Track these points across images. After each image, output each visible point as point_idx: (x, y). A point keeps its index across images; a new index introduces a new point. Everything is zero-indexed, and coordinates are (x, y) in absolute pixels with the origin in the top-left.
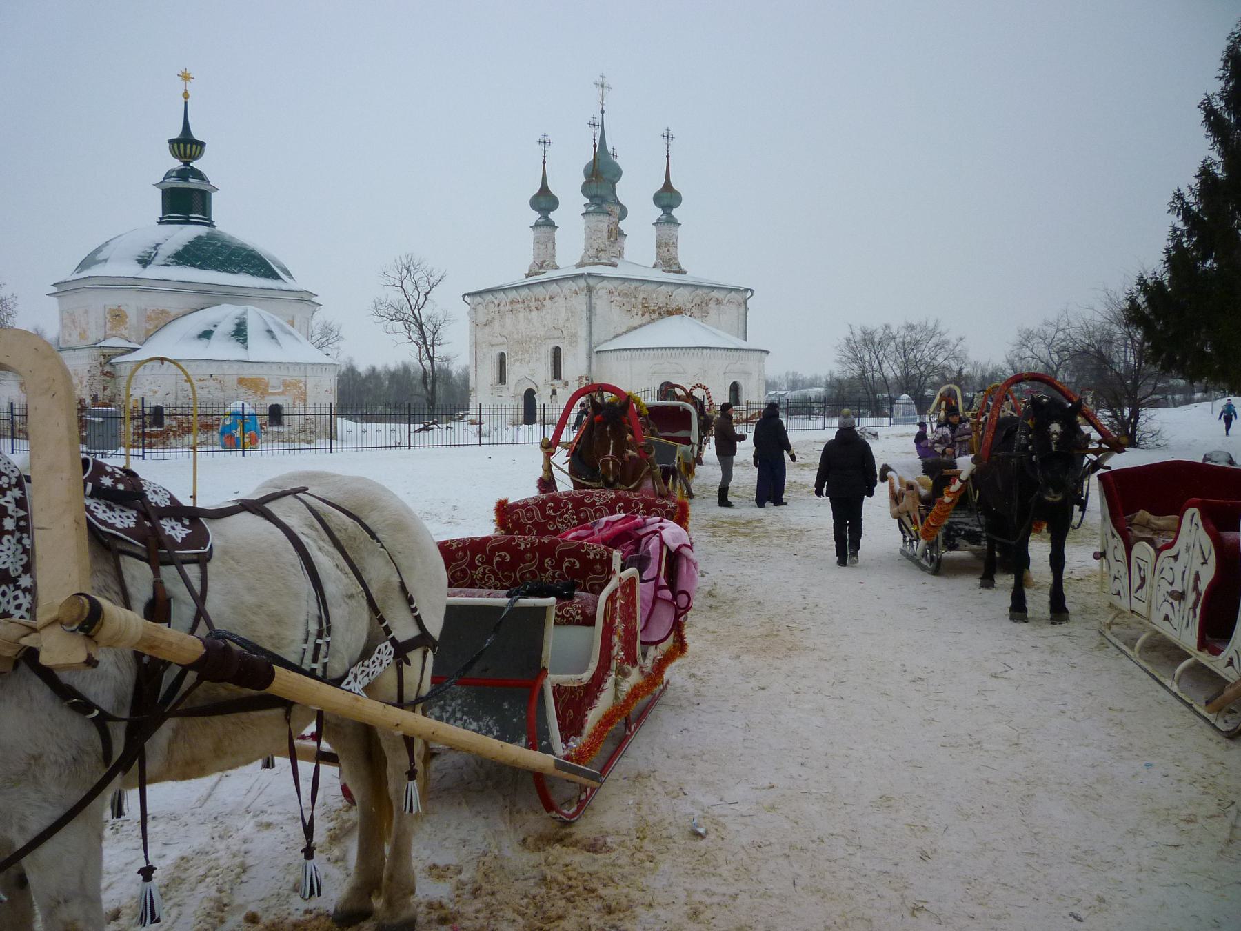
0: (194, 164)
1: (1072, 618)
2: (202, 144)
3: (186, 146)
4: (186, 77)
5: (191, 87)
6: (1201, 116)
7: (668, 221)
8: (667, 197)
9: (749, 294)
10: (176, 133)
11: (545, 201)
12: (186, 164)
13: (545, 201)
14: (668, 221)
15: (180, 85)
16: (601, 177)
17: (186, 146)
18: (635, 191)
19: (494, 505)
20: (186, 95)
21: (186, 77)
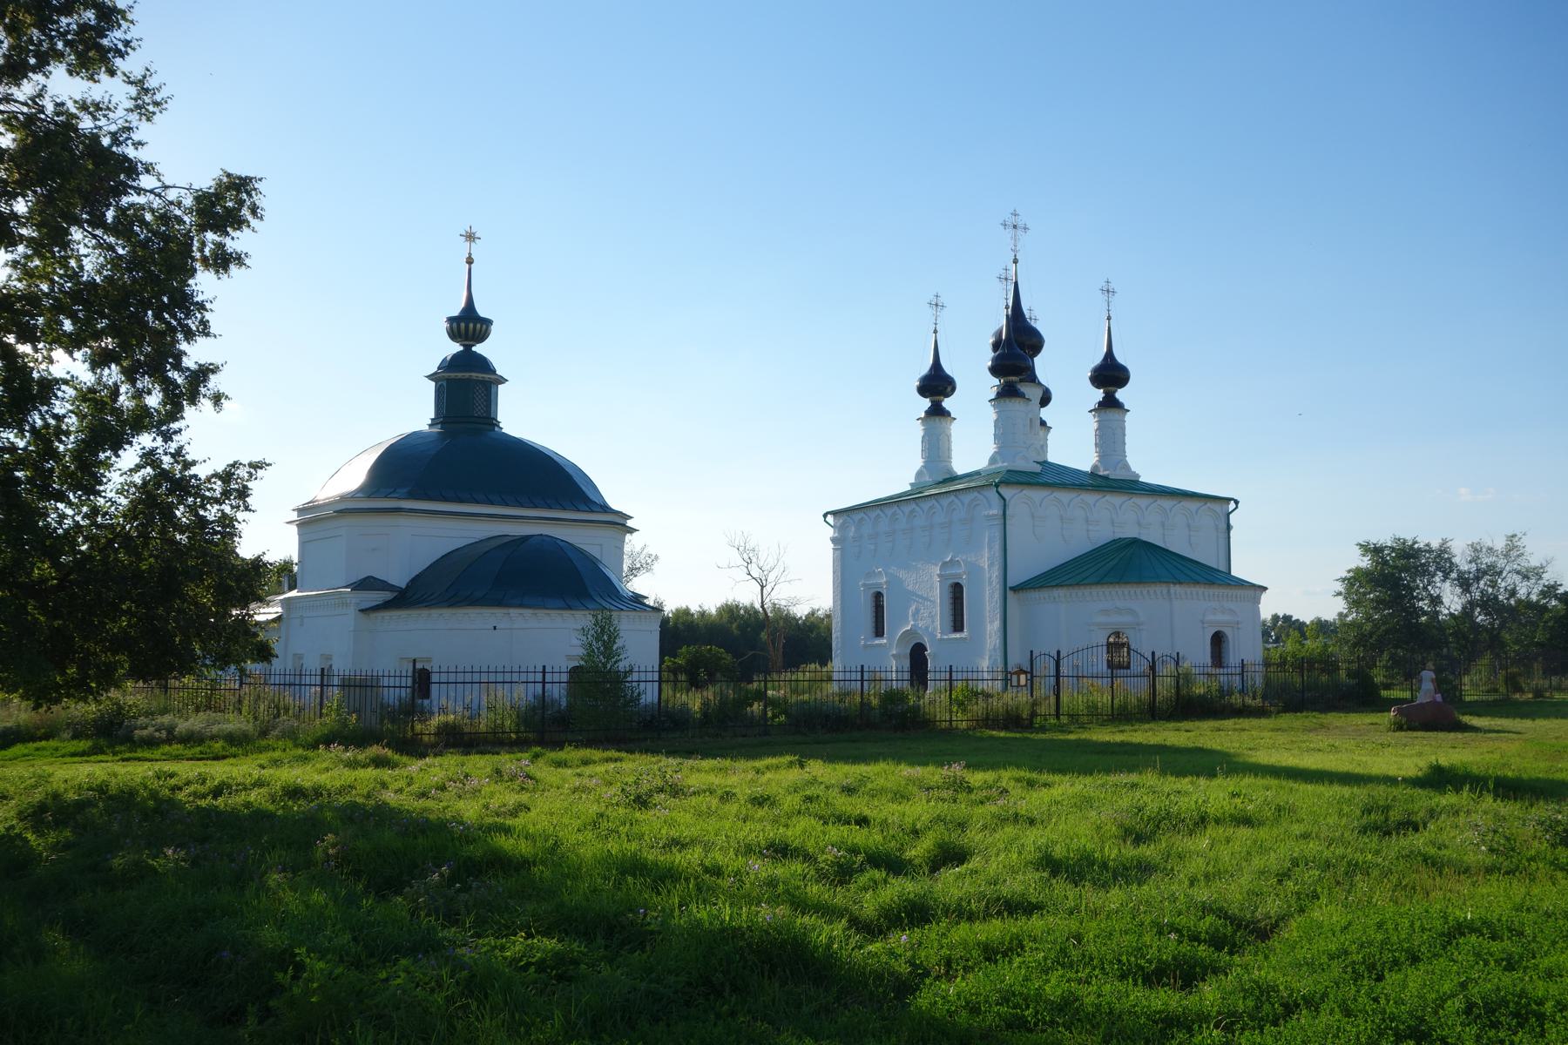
0: (478, 348)
2: (488, 322)
4: (470, 237)
8: (1110, 375)
9: (1232, 505)
10: (456, 309)
11: (936, 385)
12: (468, 348)
13: (936, 385)
15: (463, 248)
20: (470, 261)
21: (470, 237)
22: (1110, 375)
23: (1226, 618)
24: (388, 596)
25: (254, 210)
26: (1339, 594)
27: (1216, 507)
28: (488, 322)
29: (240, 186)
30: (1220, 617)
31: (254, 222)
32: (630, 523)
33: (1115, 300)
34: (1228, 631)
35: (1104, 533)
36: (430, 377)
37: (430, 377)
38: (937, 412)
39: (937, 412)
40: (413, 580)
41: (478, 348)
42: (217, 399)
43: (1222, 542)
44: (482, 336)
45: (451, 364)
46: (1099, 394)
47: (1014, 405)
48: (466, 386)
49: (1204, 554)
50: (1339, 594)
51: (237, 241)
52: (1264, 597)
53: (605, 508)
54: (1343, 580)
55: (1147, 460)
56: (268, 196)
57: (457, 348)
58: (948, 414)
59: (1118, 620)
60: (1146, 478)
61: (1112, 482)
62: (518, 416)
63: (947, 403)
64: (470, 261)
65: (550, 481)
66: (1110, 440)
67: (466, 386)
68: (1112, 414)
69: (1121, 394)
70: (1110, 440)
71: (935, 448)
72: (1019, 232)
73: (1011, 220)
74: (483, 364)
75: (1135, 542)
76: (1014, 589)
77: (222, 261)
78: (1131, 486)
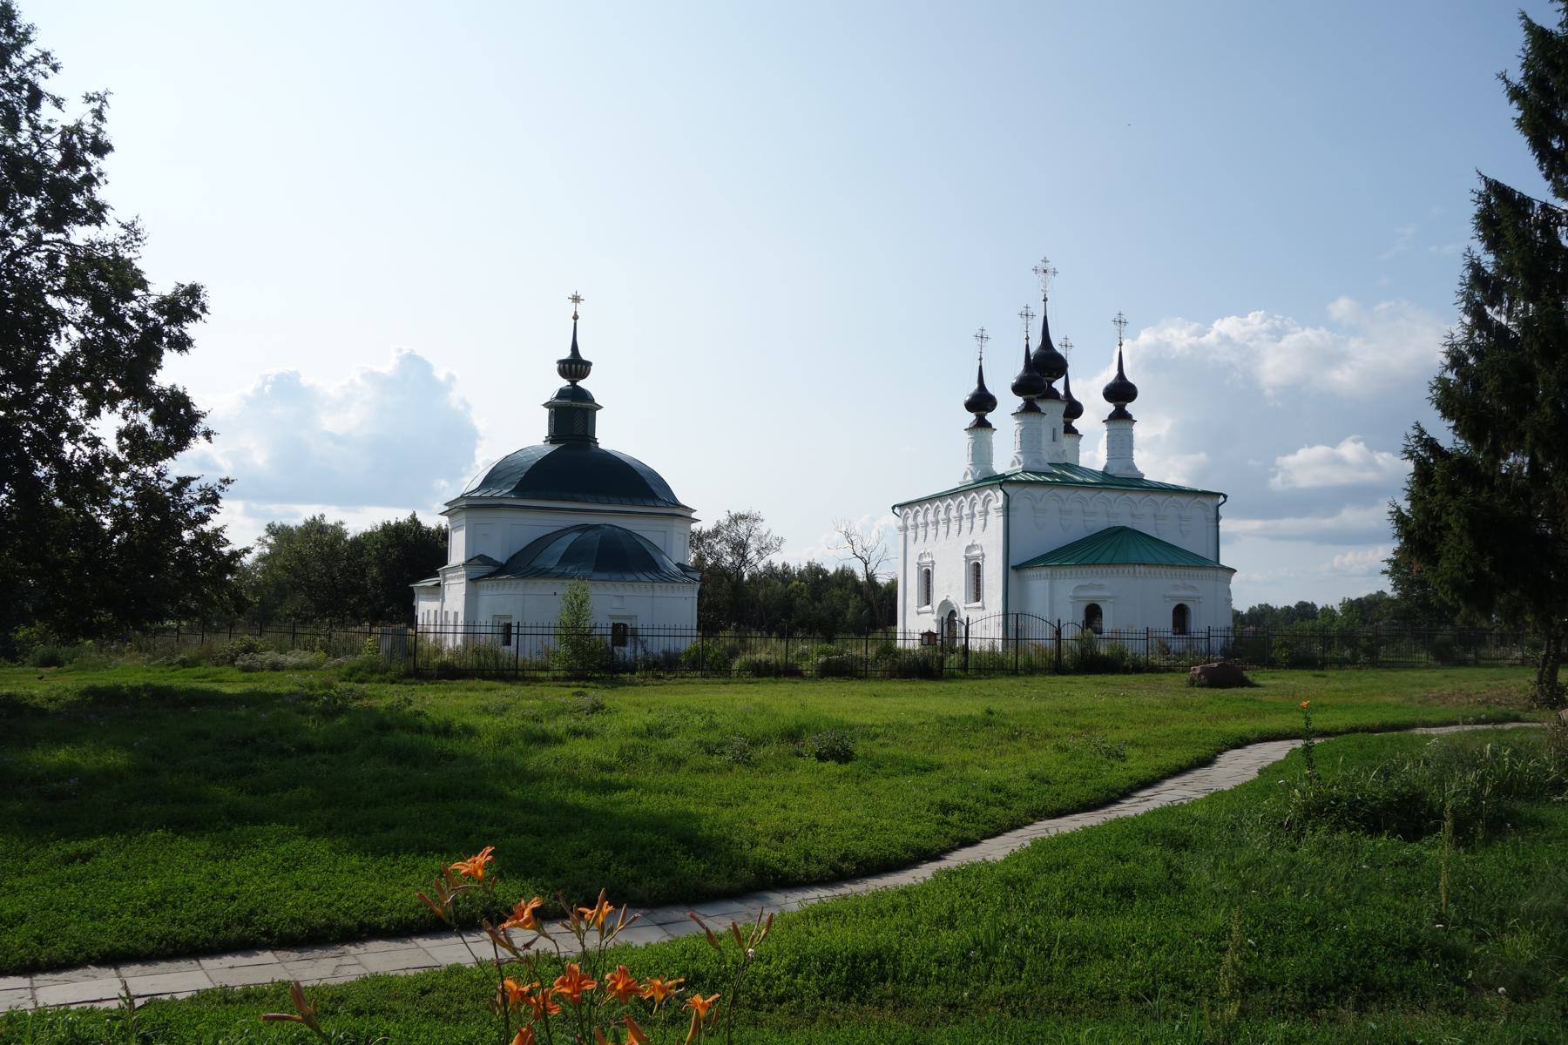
0: (581, 384)
1: (918, 637)
2: (589, 364)
3: (574, 367)
4: (576, 299)
5: (581, 308)
6: (754, 512)
7: (1120, 417)
8: (1121, 392)
9: (1222, 499)
10: (566, 354)
11: (981, 402)
12: (573, 383)
13: (981, 402)
14: (1120, 417)
15: (571, 307)
16: (1043, 372)
17: (574, 367)
18: (1087, 385)
19: (113, 143)
20: (576, 318)
21: (576, 299)
22: (1121, 392)
23: (1189, 593)
24: (492, 569)
25: (203, 309)
26: (1384, 572)
27: (1207, 501)
28: (589, 364)
29: (193, 292)
30: (1182, 593)
31: (204, 316)
32: (694, 515)
33: (988, 345)
34: (1189, 604)
35: (1100, 523)
36: (546, 405)
37: (546, 405)
38: (982, 424)
39: (982, 424)
40: (513, 558)
41: (581, 384)
42: (208, 435)
43: (1213, 530)
44: (584, 375)
45: (562, 394)
46: (1111, 408)
47: (1032, 418)
48: (572, 413)
49: (1194, 543)
50: (1384, 572)
51: (191, 329)
52: (1235, 578)
53: (677, 505)
54: (1389, 561)
55: (1151, 463)
56: (210, 297)
57: (565, 383)
58: (989, 425)
59: (1093, 595)
60: (1151, 475)
61: (1122, 481)
62: (614, 434)
63: (989, 417)
64: (576, 318)
65: (637, 486)
66: (1121, 445)
67: (572, 413)
68: (983, 432)
69: (1129, 407)
70: (1121, 445)
71: (981, 454)
72: (1049, 275)
73: (1041, 266)
74: (584, 396)
75: (1122, 530)
76: (1017, 568)
77: (182, 344)
78: (1134, 484)
